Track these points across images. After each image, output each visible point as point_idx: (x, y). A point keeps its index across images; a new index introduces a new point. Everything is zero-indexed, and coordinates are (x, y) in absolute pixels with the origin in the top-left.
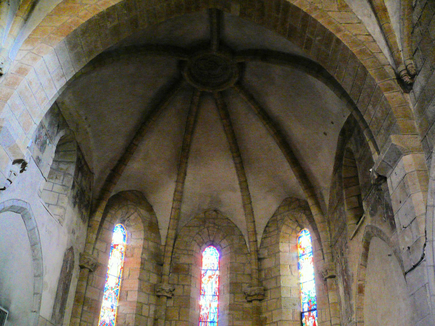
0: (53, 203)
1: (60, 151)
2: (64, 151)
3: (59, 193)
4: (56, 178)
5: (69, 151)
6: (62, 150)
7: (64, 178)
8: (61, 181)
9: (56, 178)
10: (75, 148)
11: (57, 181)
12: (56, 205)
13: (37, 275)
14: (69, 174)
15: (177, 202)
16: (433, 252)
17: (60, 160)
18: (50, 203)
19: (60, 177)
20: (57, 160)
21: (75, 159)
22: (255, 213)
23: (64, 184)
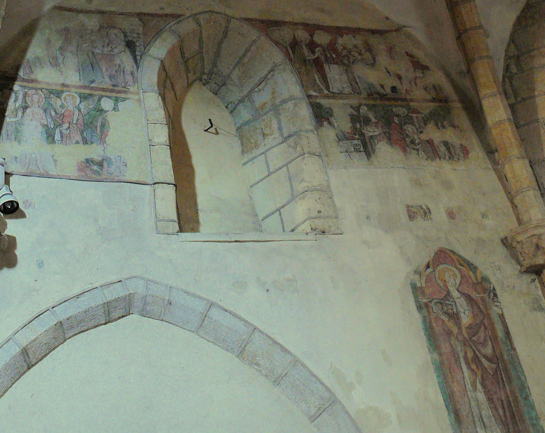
0: (284, 202)
1: (231, 73)
2: (235, 67)
3: (286, 165)
4: (264, 135)
5: (244, 55)
6: (231, 67)
7: (279, 123)
8: (277, 134)
9: (264, 135)
10: (253, 34)
11: (269, 141)
12: (293, 198)
13: (313, 411)
14: (284, 101)
15: (350, 131)
16: (176, 97)
17: (245, 92)
18: (279, 205)
19: (270, 127)
20: (242, 95)
21: (278, 56)
22: (527, 379)
23: (286, 135)
